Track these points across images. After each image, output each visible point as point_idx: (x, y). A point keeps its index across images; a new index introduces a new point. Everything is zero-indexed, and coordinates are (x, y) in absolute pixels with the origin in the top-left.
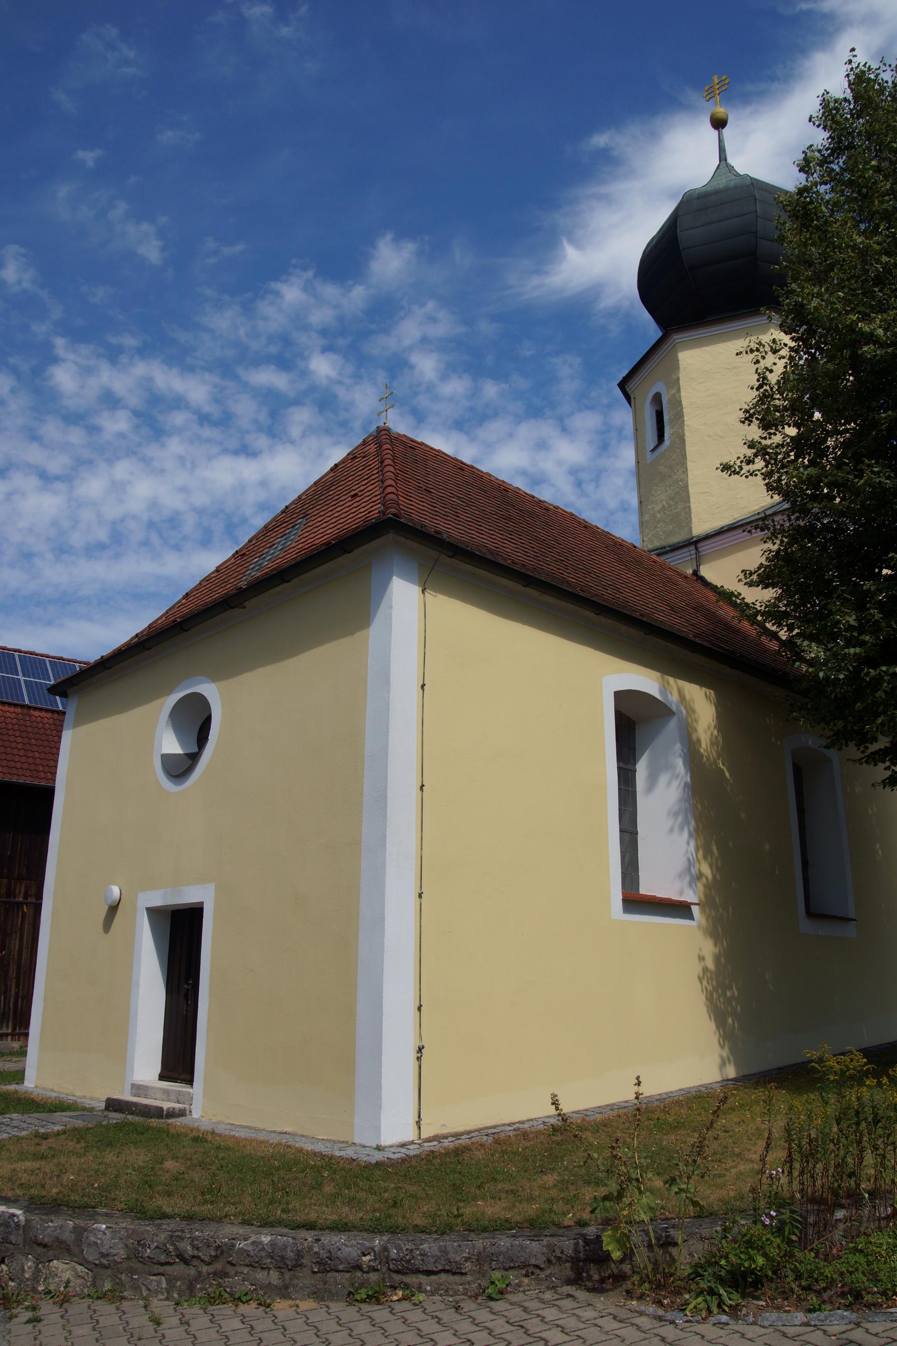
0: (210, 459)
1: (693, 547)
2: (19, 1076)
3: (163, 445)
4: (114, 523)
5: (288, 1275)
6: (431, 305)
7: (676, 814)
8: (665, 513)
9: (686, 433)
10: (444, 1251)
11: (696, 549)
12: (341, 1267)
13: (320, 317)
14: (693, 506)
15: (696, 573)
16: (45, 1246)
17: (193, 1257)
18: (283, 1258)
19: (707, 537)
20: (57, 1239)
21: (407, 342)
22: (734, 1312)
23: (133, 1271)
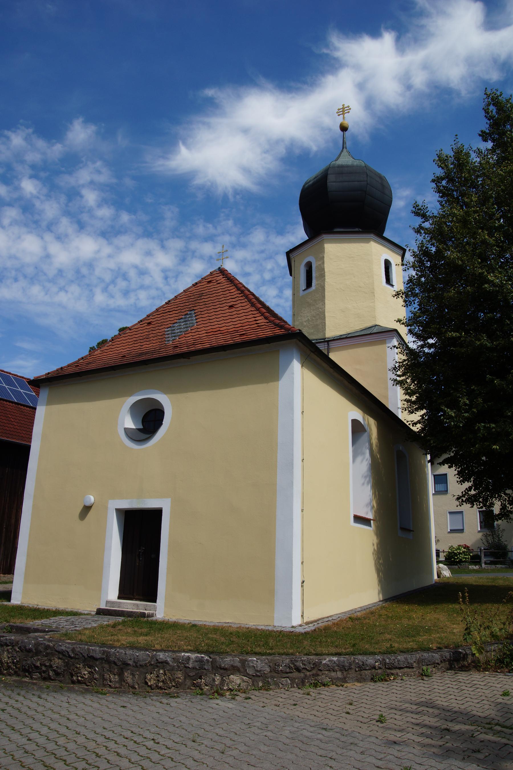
1: (326, 343)
5: (345, 673)
6: (99, 164)
7: (366, 477)
8: (309, 323)
9: (326, 285)
10: (406, 659)
11: (328, 344)
12: (367, 668)
13: (33, 157)
14: (326, 322)
16: (225, 669)
17: (303, 668)
18: (343, 666)
19: (334, 340)
20: (232, 666)
21: (81, 182)
23: (273, 677)
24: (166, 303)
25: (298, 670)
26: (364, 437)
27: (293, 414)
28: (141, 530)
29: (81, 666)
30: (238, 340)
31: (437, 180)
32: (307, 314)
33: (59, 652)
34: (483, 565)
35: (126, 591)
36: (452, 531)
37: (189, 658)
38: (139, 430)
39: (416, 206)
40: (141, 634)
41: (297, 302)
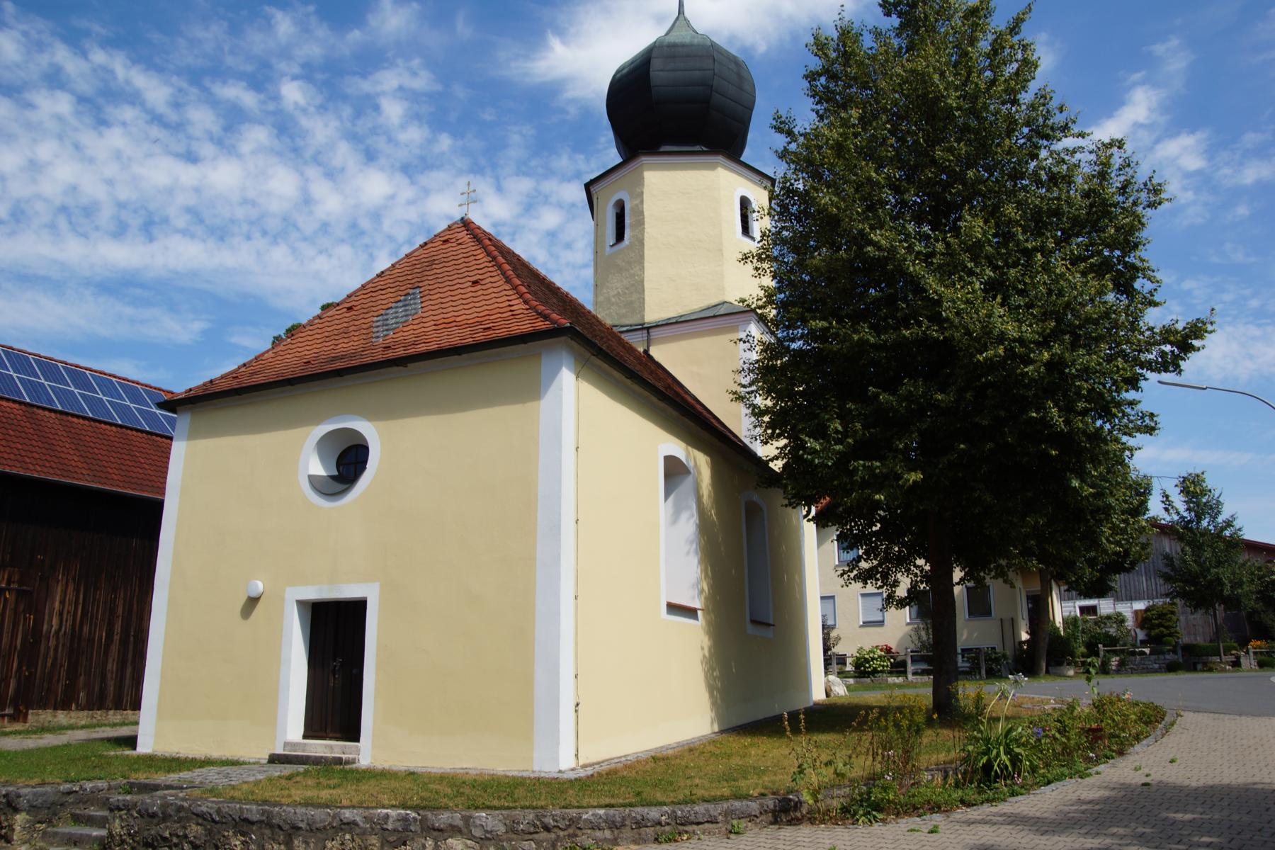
0: (149, 155)
2: (131, 742)
3: (101, 135)
4: (18, 201)
5: (616, 832)
10: (707, 810)
13: (313, 51)
15: (646, 352)
16: (440, 830)
18: (613, 822)
20: (450, 825)
22: (883, 821)
23: (510, 840)
24: (378, 276)
25: (547, 829)
26: (686, 485)
27: (560, 451)
28: (336, 633)
29: (231, 833)
30: (480, 337)
31: (812, 77)
32: (616, 284)
33: (197, 815)
34: (910, 677)
35: (313, 728)
36: (867, 624)
37: (387, 816)
38: (332, 477)
39: (777, 117)
40: (329, 787)
41: (602, 265)
